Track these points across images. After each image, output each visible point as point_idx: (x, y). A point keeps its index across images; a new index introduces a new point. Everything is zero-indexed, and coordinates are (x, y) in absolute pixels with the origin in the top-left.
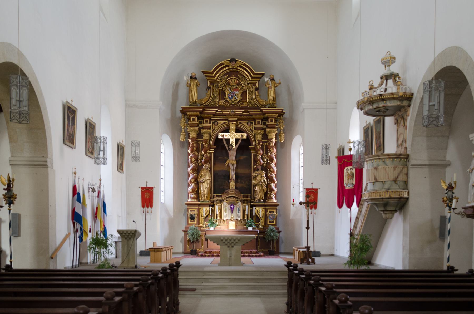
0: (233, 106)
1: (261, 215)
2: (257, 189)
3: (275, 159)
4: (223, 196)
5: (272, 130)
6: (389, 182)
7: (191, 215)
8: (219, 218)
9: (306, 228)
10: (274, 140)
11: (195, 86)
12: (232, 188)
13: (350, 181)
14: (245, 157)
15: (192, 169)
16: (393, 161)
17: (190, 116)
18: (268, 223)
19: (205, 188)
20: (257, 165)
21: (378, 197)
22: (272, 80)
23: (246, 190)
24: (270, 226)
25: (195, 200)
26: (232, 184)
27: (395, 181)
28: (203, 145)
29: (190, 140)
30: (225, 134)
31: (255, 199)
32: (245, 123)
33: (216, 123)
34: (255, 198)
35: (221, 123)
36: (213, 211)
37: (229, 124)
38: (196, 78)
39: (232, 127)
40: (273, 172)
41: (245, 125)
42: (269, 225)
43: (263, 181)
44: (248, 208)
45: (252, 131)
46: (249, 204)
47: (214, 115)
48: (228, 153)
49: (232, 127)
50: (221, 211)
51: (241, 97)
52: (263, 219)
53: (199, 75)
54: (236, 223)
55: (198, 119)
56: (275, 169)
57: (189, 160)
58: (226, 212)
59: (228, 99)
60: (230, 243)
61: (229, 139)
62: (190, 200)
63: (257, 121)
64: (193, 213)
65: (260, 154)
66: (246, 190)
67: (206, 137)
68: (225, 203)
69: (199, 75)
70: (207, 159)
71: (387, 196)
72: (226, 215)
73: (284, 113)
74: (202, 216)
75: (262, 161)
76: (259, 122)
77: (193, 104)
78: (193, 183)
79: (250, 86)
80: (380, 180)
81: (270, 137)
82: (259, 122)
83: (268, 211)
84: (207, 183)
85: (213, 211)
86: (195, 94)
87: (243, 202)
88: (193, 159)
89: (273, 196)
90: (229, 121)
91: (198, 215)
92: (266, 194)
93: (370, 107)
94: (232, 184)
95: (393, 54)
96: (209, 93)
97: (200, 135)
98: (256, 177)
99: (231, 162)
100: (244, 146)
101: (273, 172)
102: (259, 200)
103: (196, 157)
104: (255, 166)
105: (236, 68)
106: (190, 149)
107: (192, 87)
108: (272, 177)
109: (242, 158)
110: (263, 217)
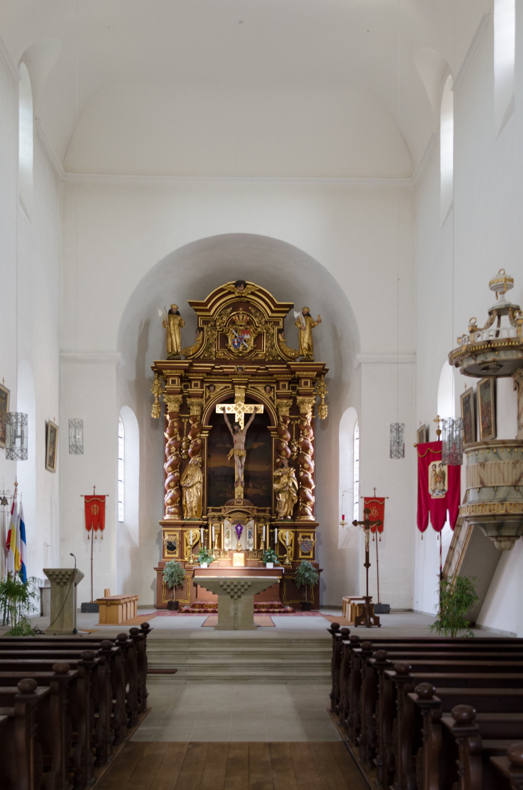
0: (240, 360)
1: (288, 544)
2: (282, 498)
3: (311, 447)
5: (307, 398)
6: (505, 488)
7: (170, 543)
8: (216, 548)
9: (365, 565)
10: (309, 416)
13: (439, 486)
14: (261, 444)
15: (171, 465)
16: (511, 452)
19: (193, 496)
20: (280, 458)
21: (487, 513)
22: (307, 315)
23: (262, 500)
24: (303, 561)
25: (176, 517)
26: (239, 490)
27: (515, 486)
28: (191, 425)
29: (168, 417)
30: (226, 406)
31: (277, 515)
34: (277, 514)
36: (206, 535)
37: (233, 388)
38: (178, 313)
39: (240, 394)
40: (309, 469)
41: (261, 392)
42: (301, 559)
43: (291, 484)
44: (265, 530)
45: (273, 401)
46: (268, 524)
49: (240, 394)
51: (254, 344)
52: (292, 549)
53: (183, 307)
54: (246, 557)
55: (182, 381)
56: (312, 464)
57: (167, 449)
58: (228, 537)
59: (232, 348)
60: (236, 590)
62: (167, 517)
63: (281, 383)
64: (172, 539)
65: (286, 439)
66: (262, 500)
67: (195, 411)
68: (226, 523)
69: (183, 307)
71: (503, 512)
74: (187, 545)
75: (289, 451)
76: (284, 386)
77: (174, 356)
78: (173, 488)
79: (269, 326)
80: (489, 485)
81: (302, 411)
82: (284, 386)
83: (301, 535)
84: (197, 489)
85: (206, 535)
86: (176, 339)
87: (257, 519)
88: (173, 449)
89: (309, 510)
91: (181, 543)
92: (296, 507)
93: (472, 362)
94: (239, 490)
95: (509, 273)
97: (184, 408)
98: (279, 477)
99: (236, 453)
100: (259, 425)
101: (309, 469)
102: (285, 517)
103: (179, 444)
104: (278, 460)
105: (245, 297)
107: (172, 328)
108: (307, 479)
109: (256, 446)
110: (291, 545)
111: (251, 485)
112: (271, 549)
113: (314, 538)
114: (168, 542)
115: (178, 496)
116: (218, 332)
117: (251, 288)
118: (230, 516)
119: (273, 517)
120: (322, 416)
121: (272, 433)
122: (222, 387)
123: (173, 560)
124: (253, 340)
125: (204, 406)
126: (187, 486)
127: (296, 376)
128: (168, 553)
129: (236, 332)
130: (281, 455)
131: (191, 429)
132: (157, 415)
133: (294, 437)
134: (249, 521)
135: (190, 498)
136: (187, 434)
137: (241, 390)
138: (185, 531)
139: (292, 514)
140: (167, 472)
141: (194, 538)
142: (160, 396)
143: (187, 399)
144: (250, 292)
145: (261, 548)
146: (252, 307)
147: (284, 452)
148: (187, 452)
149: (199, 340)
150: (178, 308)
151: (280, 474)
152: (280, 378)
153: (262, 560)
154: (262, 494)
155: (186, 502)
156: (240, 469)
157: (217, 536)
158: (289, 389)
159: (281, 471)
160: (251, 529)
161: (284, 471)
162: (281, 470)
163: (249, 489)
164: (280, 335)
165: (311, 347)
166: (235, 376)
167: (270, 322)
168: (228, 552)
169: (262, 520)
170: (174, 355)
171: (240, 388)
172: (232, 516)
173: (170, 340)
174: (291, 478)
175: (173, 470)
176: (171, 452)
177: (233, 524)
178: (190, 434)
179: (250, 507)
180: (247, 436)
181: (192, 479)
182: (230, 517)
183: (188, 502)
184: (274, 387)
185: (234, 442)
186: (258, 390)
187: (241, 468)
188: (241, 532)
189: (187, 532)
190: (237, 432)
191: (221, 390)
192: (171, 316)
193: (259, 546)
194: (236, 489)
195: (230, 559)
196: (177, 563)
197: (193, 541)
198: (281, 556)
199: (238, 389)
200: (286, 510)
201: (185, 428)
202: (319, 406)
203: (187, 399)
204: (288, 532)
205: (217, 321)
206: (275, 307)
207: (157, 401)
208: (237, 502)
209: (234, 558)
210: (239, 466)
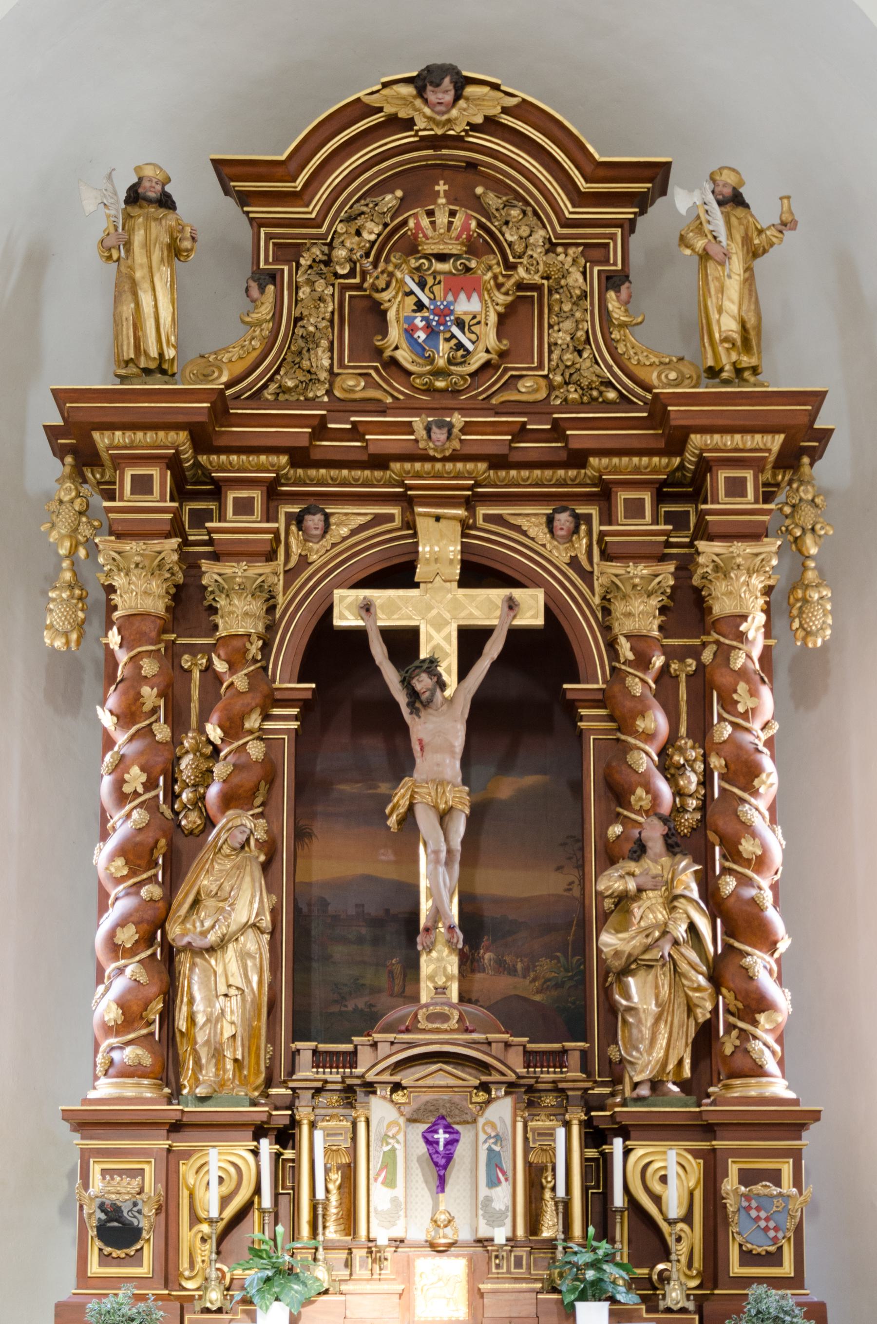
0: (440, 399)
1: (674, 1210)
2: (640, 993)
3: (767, 762)
4: (365, 1057)
5: (742, 549)
7: (112, 1212)
8: (332, 1232)
10: (754, 627)
11: (156, 256)
12: (441, 990)
14: (530, 780)
15: (123, 851)
17: (120, 462)
18: (736, 1269)
19: (226, 993)
20: (626, 821)
22: (734, 200)
23: (553, 1009)
24: (755, 1290)
26: (439, 966)
28: (218, 679)
29: (114, 638)
30: (378, 596)
31: (617, 1080)
32: (531, 519)
33: (314, 521)
34: (615, 1072)
35: (347, 519)
36: (285, 1172)
37: (410, 525)
38: (166, 202)
39: (439, 545)
40: (760, 863)
42: (747, 1281)
43: (681, 931)
44: (566, 1146)
45: (587, 577)
46: (576, 1116)
47: (300, 457)
48: (404, 729)
49: (439, 545)
50: (349, 1172)
51: (499, 336)
54: (474, 1275)
56: (775, 842)
57: (107, 781)
58: (390, 1183)
59: (404, 356)
61: (413, 634)
62: (105, 1088)
63: (622, 496)
64: (121, 1191)
65: (649, 737)
66: (553, 1009)
67: (239, 616)
68: (381, 1110)
70: (247, 779)
72: (397, 1203)
73: (825, 435)
74: (195, 1219)
75: (664, 789)
78: (131, 953)
81: (721, 607)
82: (635, 509)
83: (733, 1169)
84: (243, 956)
85: (285, 1172)
86: (158, 303)
87: (528, 1096)
88: (136, 777)
89: (765, 1048)
90: (407, 501)
91: (166, 1208)
92: (705, 1039)
94: (439, 966)
96: (265, 310)
97: (189, 604)
98: (623, 901)
99: (425, 796)
100: (531, 690)
101: (760, 863)
102: (656, 1084)
103: (160, 760)
104: (616, 830)
105: (458, 141)
106: (112, 701)
109: (506, 788)
110: (688, 1219)
111: (488, 957)
112: (599, 1238)
113: (797, 1182)
114: (102, 1207)
115: (154, 990)
116: (344, 288)
117: (481, 98)
118: (396, 1078)
119: (597, 1091)
120: (808, 633)
121: (583, 712)
122: (362, 520)
123: (123, 1293)
124: (493, 318)
125: (281, 601)
126: (198, 943)
127: (690, 457)
128: (105, 1259)
129: (422, 285)
130: (628, 806)
131: (219, 697)
132: (66, 634)
133: (683, 731)
134: (489, 1102)
135: (210, 1003)
136: (204, 718)
137: (443, 522)
138: (187, 1155)
139: (687, 1072)
140: (108, 885)
141: (226, 1189)
142: (82, 552)
143: (205, 565)
144: (479, 120)
145: (546, 1234)
146: (487, 188)
147: (640, 792)
148: (203, 798)
149: (259, 323)
150: (169, 180)
151: (632, 885)
152: (616, 471)
153: (555, 1290)
154: (538, 998)
155: (192, 1019)
156: (442, 869)
157: (336, 1177)
158: (656, 521)
159: (632, 874)
160: (498, 1138)
161: (646, 872)
162: (632, 866)
163: (479, 976)
164: (611, 295)
165: (752, 334)
166: (418, 466)
167: (566, 246)
168: (389, 1253)
169: (549, 1100)
170: (147, 371)
171: (438, 518)
172: (407, 1077)
173: (127, 309)
174: (681, 903)
175: (133, 873)
176: (127, 789)
177: (411, 1120)
178: (215, 717)
179: (492, 1036)
180: (473, 724)
181: (221, 910)
182: (397, 1087)
183: (200, 1019)
184: (588, 518)
185: (416, 747)
186: (518, 529)
187: (448, 863)
188: (449, 1158)
189: (195, 1162)
190: (427, 704)
191: (354, 532)
192: (135, 211)
193: (534, 1225)
194: (423, 959)
195: (399, 1288)
196: (142, 1306)
197: (225, 1201)
198: (642, 1272)
199: (432, 521)
200: (658, 1053)
201: (195, 694)
202: (794, 588)
203: (205, 565)
204: (672, 1156)
205: (336, 243)
206: (574, 206)
207: (68, 576)
208: (431, 1018)
209: (419, 1282)
210: (437, 852)
